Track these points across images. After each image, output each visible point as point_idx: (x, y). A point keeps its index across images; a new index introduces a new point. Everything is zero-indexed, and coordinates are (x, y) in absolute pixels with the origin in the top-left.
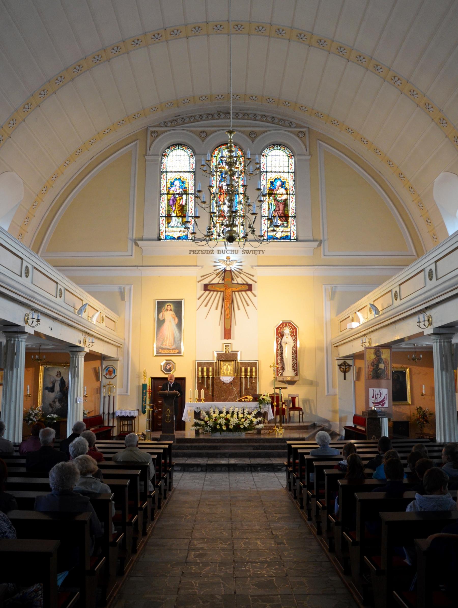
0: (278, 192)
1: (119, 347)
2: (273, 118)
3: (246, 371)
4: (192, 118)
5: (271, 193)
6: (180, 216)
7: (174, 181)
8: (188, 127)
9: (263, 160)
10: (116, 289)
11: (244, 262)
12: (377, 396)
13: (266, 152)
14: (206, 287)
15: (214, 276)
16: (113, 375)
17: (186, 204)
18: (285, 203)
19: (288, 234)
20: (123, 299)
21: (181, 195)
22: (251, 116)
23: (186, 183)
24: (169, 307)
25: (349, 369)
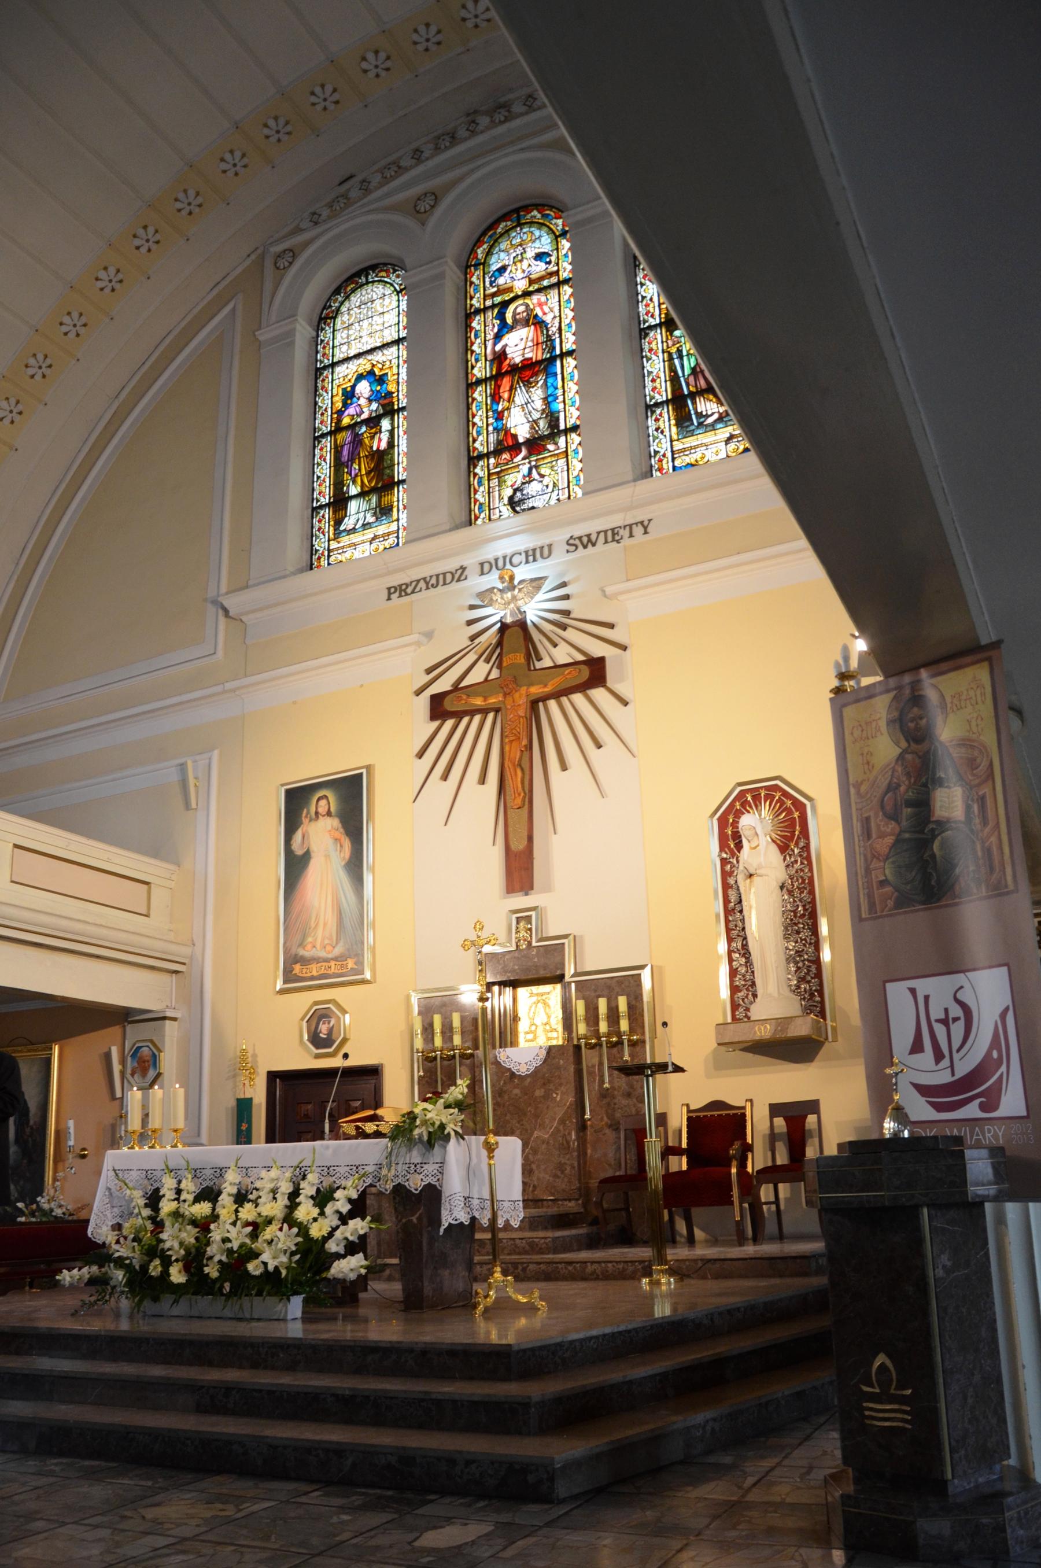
1: (176, 972)
7: (353, 387)
8: (380, 199)
11: (576, 579)
12: (940, 1030)
14: (439, 708)
16: (151, 1074)
17: (391, 444)
21: (373, 422)
24: (323, 802)
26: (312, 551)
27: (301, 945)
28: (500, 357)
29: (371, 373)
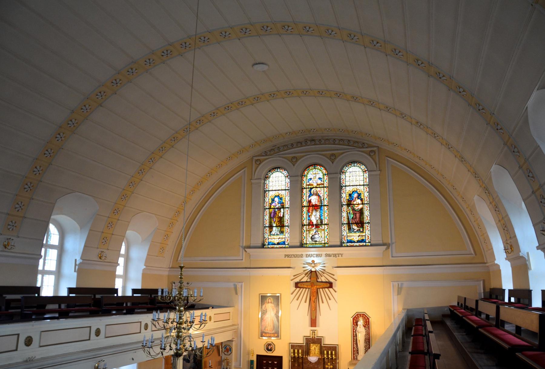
0: (355, 203)
2: (349, 141)
4: (286, 147)
5: (349, 204)
6: (279, 226)
8: (283, 154)
9: (343, 176)
10: (231, 285)
13: (345, 169)
14: (297, 285)
15: (304, 275)
16: (229, 352)
18: (361, 211)
19: (364, 238)
21: (279, 209)
26: (264, 237)
28: (310, 202)
29: (278, 196)
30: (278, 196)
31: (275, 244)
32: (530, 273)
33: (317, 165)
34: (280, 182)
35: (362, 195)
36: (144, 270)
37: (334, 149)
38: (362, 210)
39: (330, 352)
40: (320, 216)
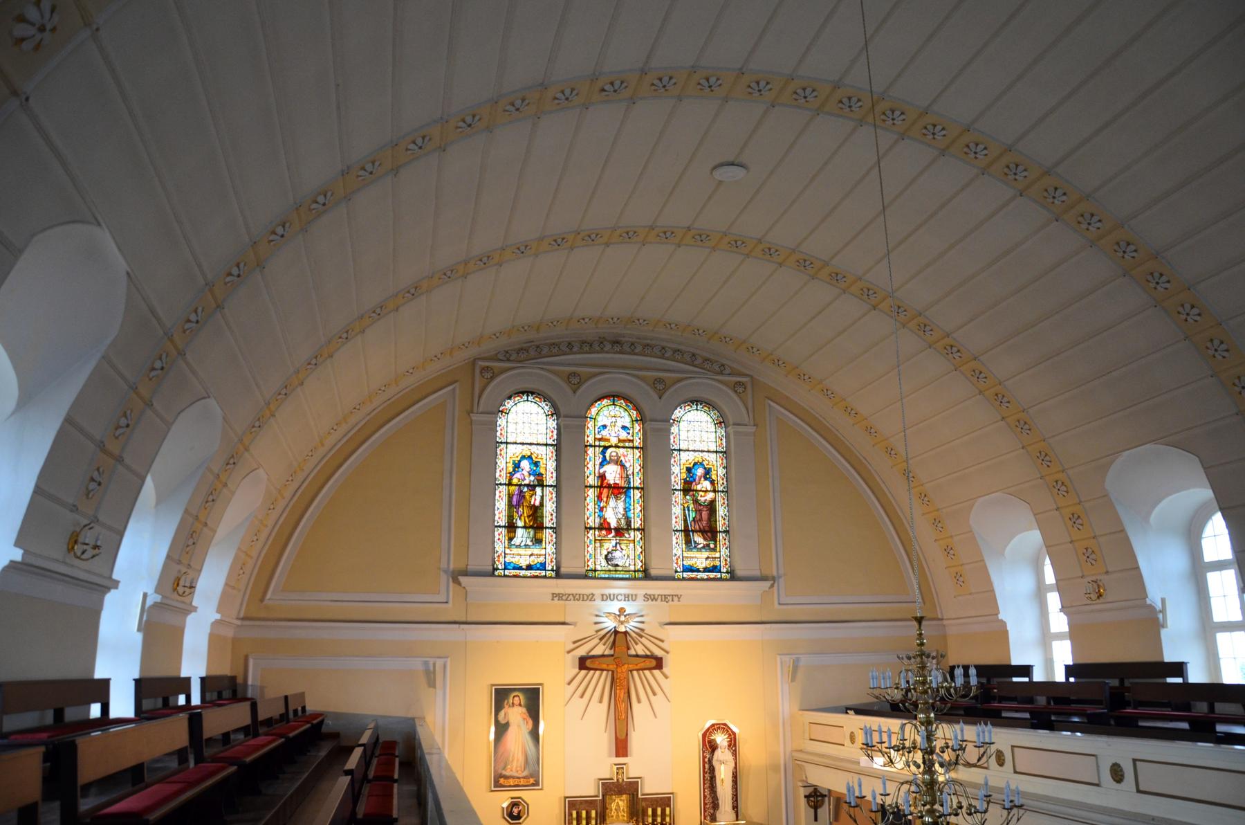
0: (699, 487)
2: (694, 355)
3: (654, 814)
5: (687, 489)
10: (417, 664)
14: (583, 663)
15: (596, 641)
17: (542, 504)
18: (711, 506)
19: (717, 563)
20: (432, 684)
21: (532, 487)
22: (687, 358)
23: (542, 465)
25: (823, 802)
27: (504, 768)
28: (602, 477)
29: (530, 457)
30: (530, 457)
31: (520, 568)
32: (1164, 633)
33: (620, 397)
34: (536, 427)
35: (714, 472)
36: (216, 624)
37: (652, 363)
38: (713, 502)
39: (659, 811)
40: (626, 510)
